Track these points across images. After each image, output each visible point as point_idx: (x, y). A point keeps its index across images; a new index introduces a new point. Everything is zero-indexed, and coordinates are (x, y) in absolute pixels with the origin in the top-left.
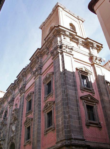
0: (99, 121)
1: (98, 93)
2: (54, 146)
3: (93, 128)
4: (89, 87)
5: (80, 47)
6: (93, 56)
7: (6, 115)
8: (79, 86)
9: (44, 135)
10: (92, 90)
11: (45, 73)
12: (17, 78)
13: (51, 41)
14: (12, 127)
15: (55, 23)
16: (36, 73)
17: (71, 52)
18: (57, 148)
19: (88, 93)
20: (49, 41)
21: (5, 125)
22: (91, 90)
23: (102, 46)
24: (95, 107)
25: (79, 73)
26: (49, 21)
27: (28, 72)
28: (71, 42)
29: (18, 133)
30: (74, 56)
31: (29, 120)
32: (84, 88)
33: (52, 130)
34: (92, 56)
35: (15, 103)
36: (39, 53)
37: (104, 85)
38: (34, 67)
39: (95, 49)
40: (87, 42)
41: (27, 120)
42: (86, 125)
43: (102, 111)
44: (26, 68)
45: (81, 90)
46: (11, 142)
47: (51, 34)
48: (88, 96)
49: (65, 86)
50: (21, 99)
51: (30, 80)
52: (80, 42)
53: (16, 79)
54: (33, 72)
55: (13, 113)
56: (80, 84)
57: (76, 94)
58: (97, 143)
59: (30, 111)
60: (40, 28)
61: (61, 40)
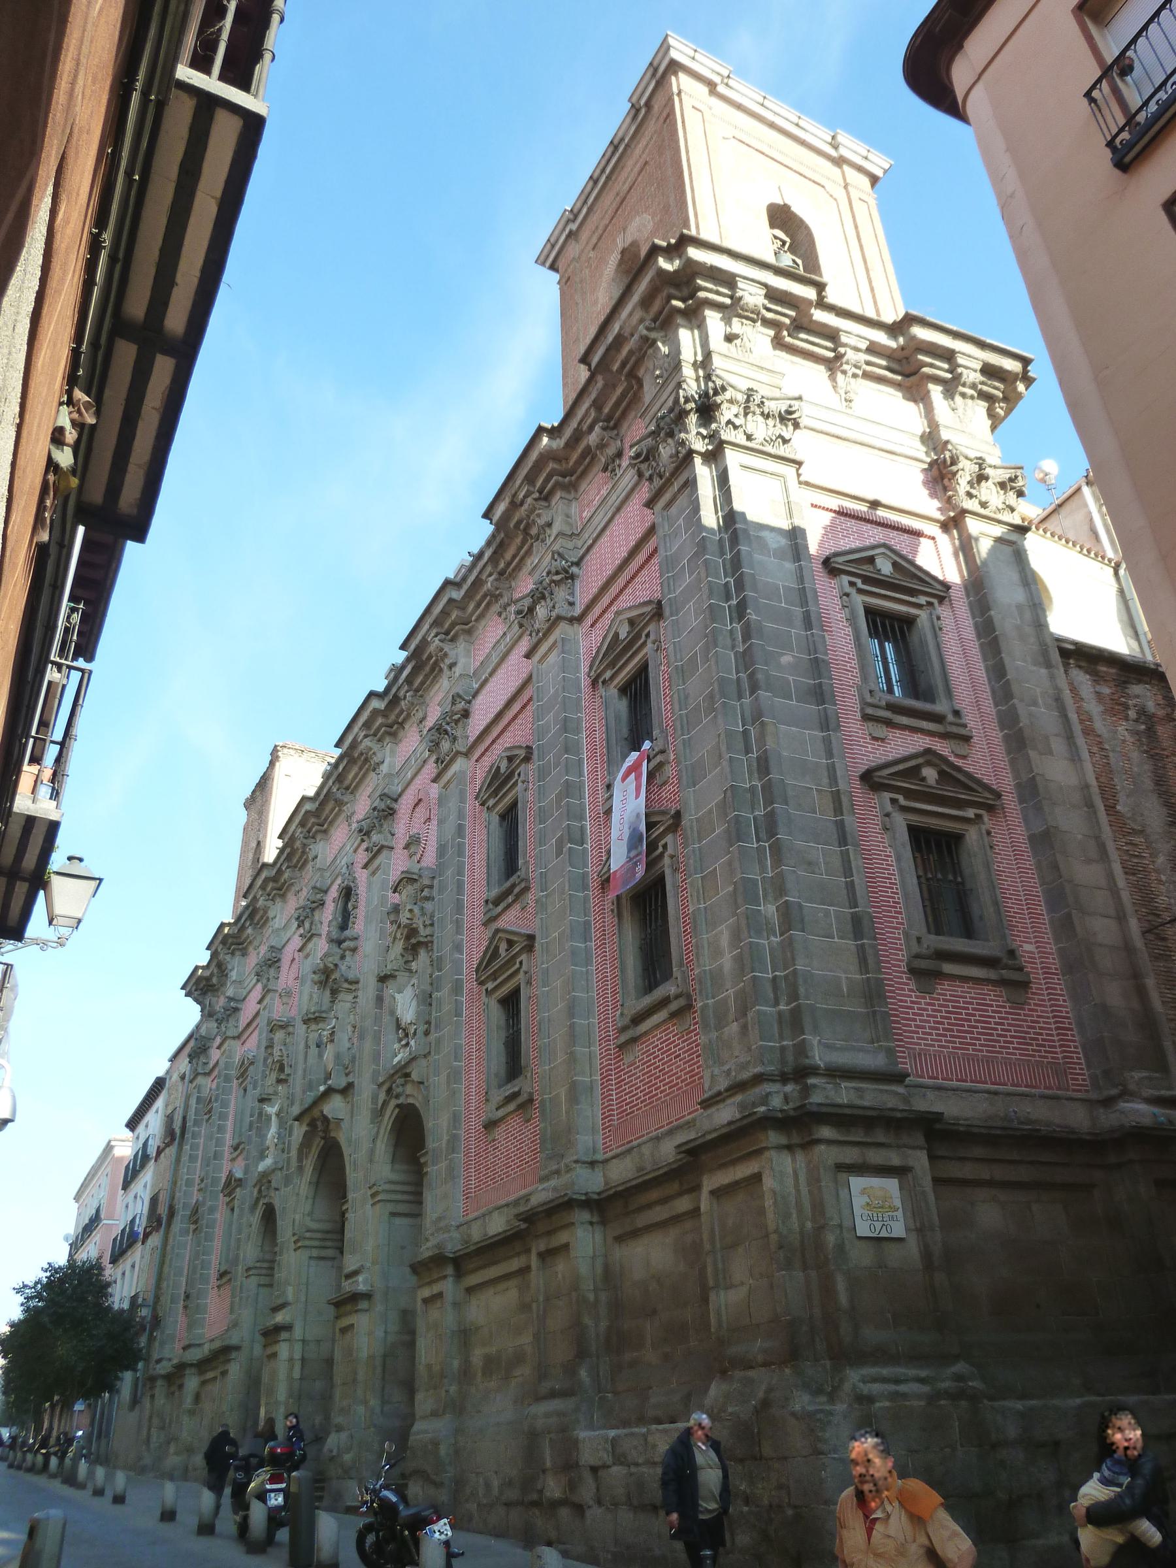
0: (1004, 937)
1: (997, 735)
2: (689, 1125)
3: (961, 989)
4: (928, 695)
5: (851, 396)
6: (954, 461)
7: (345, 919)
8: (854, 691)
9: (621, 1047)
10: (950, 718)
11: (604, 612)
12: (338, 751)
13: (628, 367)
14: (397, 996)
15: (653, 215)
16: (541, 611)
17: (785, 441)
18: (709, 1137)
19: (919, 743)
20: (616, 367)
21: (346, 985)
22: (938, 718)
23: (1025, 370)
24: (972, 836)
25: (847, 595)
26: (609, 200)
27: (478, 605)
28: (784, 359)
29: (439, 1041)
30: (807, 473)
31: (510, 943)
32: (891, 707)
33: (673, 1015)
34: (948, 454)
35: (401, 828)
36: (313, 820)
37: (1043, 671)
38: (519, 567)
39: (972, 397)
40: (906, 353)
41: (497, 948)
42: (913, 971)
43: (1029, 862)
44: (464, 579)
45: (866, 718)
46: (393, 1102)
47: (625, 314)
48: (920, 760)
49: (747, 701)
50: (441, 800)
51: (499, 664)
52: (851, 355)
53: (401, 657)
54: (513, 608)
55: (396, 898)
56: (858, 680)
57: (830, 754)
58: (996, 1093)
59: (514, 886)
60: (541, 261)
61: (708, 355)
